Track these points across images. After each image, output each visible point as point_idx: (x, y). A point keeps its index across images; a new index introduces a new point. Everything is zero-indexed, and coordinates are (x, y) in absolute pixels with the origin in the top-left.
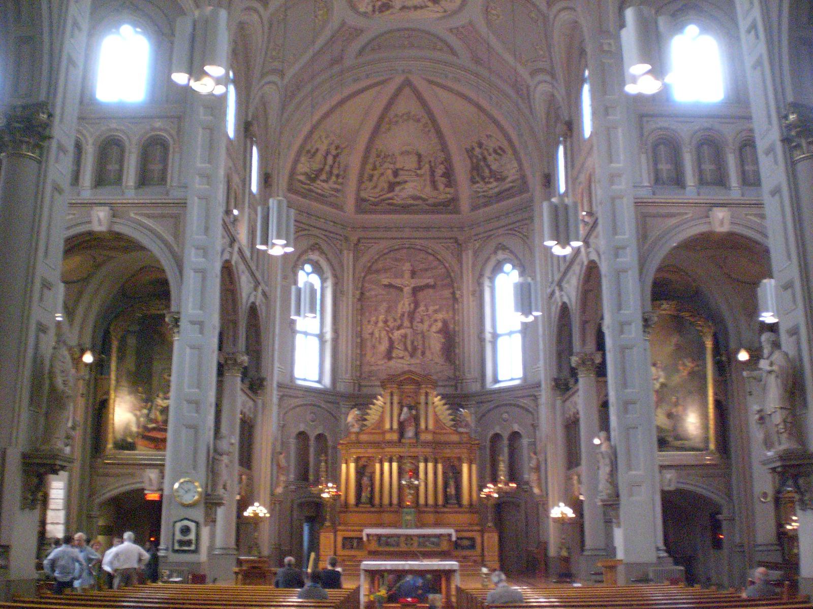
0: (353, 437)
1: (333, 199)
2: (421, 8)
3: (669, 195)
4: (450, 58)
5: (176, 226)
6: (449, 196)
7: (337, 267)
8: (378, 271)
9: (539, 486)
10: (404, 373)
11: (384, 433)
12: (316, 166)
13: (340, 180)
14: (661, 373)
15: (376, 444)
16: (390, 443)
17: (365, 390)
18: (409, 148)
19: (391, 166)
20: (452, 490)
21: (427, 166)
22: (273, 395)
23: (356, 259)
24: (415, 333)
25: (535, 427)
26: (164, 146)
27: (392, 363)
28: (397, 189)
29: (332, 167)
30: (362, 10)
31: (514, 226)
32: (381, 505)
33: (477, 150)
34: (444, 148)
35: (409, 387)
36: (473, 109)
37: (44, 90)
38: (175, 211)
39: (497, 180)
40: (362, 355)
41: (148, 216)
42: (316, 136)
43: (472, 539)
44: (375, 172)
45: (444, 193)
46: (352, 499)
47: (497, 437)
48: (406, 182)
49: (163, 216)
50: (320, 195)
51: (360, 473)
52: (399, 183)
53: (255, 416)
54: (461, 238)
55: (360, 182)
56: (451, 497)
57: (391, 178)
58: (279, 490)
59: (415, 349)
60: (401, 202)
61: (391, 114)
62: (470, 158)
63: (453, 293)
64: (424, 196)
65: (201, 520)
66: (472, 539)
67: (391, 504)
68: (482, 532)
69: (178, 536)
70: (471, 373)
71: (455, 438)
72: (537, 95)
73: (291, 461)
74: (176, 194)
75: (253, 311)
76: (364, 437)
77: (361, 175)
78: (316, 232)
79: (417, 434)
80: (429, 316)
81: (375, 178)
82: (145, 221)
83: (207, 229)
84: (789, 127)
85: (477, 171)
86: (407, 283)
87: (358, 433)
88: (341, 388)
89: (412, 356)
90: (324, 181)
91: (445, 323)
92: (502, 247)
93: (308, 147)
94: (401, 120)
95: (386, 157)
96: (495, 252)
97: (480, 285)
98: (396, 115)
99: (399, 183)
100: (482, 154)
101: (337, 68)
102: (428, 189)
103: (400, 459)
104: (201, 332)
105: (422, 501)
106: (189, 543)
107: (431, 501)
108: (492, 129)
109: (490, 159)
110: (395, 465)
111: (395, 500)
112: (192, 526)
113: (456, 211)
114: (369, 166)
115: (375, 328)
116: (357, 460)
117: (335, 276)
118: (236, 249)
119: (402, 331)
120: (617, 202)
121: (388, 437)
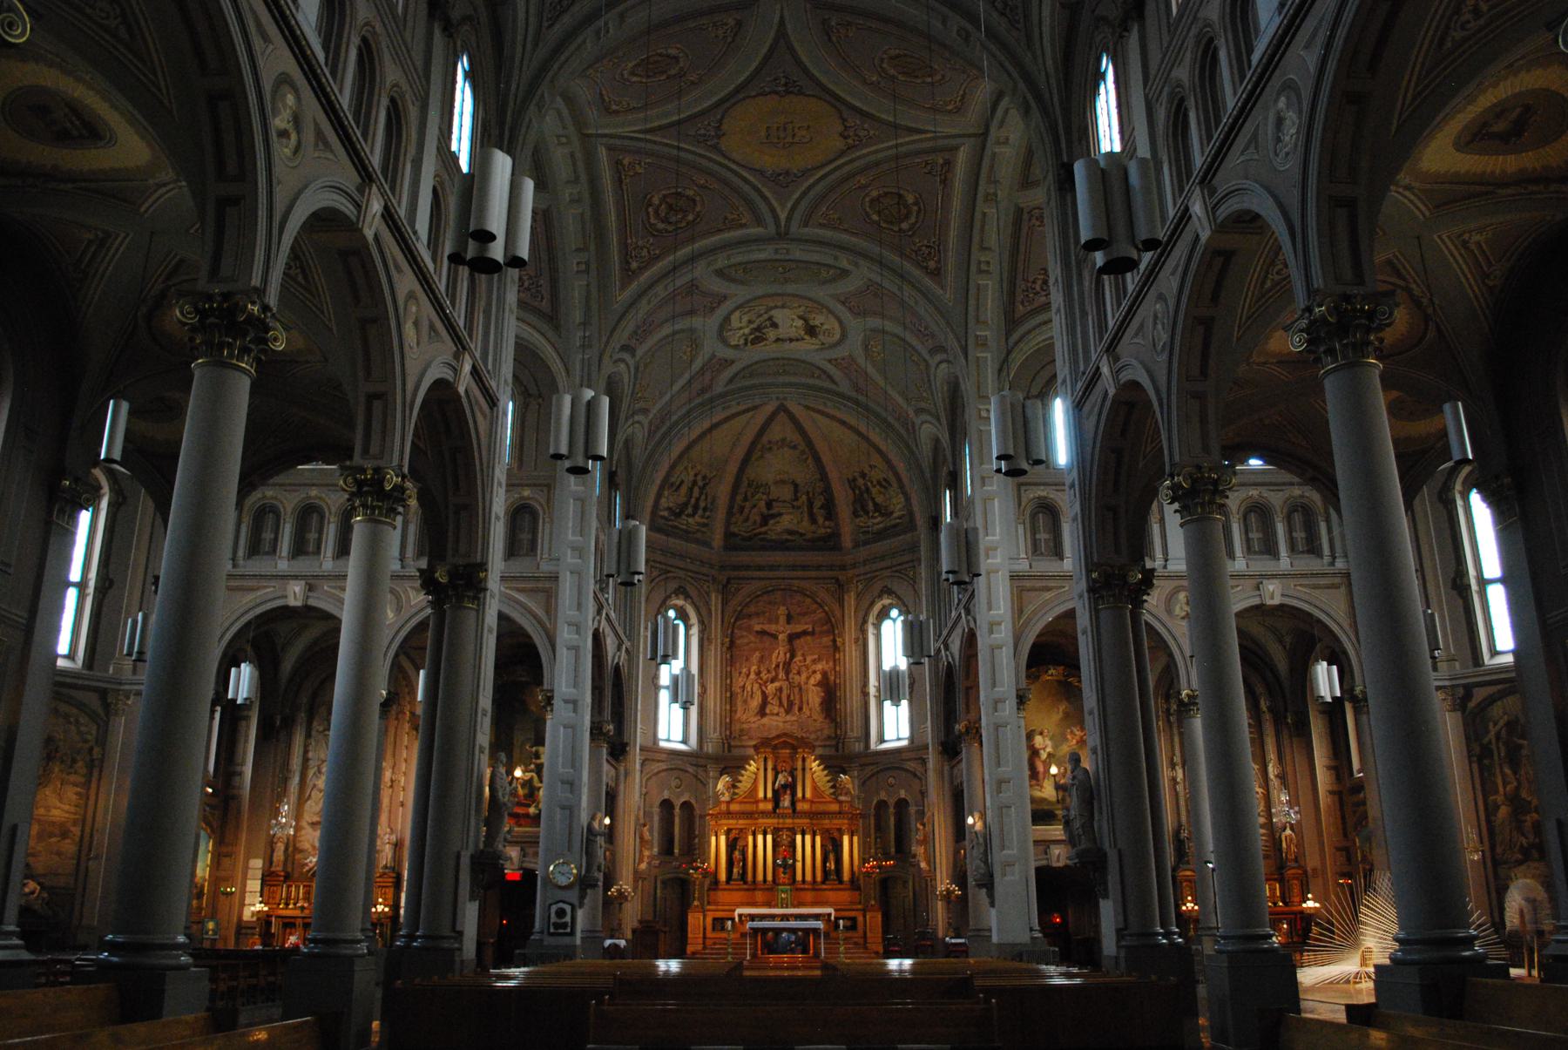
0: (724, 807)
1: (699, 535)
3: (1048, 566)
5: (549, 598)
7: (704, 613)
8: (749, 616)
9: (928, 863)
10: (778, 736)
11: (757, 802)
12: (682, 499)
14: (1049, 743)
15: (749, 815)
16: (764, 814)
17: (736, 752)
20: (832, 865)
22: (636, 757)
23: (725, 603)
24: (791, 686)
25: (923, 794)
26: (534, 515)
27: (765, 720)
29: (698, 500)
32: (754, 881)
33: (860, 481)
34: (824, 477)
35: (783, 749)
38: (547, 585)
39: (882, 515)
40: (732, 711)
41: (519, 590)
42: (680, 468)
43: (854, 920)
44: (747, 504)
46: (723, 876)
47: (882, 805)
48: (780, 515)
51: (731, 846)
52: (773, 516)
53: (617, 784)
55: (730, 513)
56: (831, 875)
57: (764, 510)
58: (643, 866)
59: (791, 704)
61: (765, 439)
63: (834, 641)
65: (576, 903)
66: (854, 920)
67: (765, 880)
68: (864, 911)
69: (553, 919)
70: (855, 732)
71: (835, 807)
73: (653, 834)
74: (546, 567)
75: (617, 669)
76: (734, 807)
77: (731, 507)
78: (681, 574)
79: (793, 803)
80: (807, 667)
82: (521, 597)
83: (579, 606)
85: (861, 505)
86: (782, 630)
87: (728, 803)
88: (709, 748)
89: (788, 711)
91: (824, 674)
92: (887, 591)
95: (758, 487)
96: (880, 596)
97: (863, 632)
101: (707, 396)
103: (776, 832)
104: (575, 711)
105: (799, 877)
106: (564, 925)
107: (809, 877)
108: (876, 459)
109: (874, 491)
110: (769, 838)
111: (770, 878)
112: (568, 908)
113: (837, 547)
114: (739, 498)
115: (747, 680)
116: (728, 832)
117: (701, 622)
118: (467, 368)
119: (777, 684)
121: (762, 806)
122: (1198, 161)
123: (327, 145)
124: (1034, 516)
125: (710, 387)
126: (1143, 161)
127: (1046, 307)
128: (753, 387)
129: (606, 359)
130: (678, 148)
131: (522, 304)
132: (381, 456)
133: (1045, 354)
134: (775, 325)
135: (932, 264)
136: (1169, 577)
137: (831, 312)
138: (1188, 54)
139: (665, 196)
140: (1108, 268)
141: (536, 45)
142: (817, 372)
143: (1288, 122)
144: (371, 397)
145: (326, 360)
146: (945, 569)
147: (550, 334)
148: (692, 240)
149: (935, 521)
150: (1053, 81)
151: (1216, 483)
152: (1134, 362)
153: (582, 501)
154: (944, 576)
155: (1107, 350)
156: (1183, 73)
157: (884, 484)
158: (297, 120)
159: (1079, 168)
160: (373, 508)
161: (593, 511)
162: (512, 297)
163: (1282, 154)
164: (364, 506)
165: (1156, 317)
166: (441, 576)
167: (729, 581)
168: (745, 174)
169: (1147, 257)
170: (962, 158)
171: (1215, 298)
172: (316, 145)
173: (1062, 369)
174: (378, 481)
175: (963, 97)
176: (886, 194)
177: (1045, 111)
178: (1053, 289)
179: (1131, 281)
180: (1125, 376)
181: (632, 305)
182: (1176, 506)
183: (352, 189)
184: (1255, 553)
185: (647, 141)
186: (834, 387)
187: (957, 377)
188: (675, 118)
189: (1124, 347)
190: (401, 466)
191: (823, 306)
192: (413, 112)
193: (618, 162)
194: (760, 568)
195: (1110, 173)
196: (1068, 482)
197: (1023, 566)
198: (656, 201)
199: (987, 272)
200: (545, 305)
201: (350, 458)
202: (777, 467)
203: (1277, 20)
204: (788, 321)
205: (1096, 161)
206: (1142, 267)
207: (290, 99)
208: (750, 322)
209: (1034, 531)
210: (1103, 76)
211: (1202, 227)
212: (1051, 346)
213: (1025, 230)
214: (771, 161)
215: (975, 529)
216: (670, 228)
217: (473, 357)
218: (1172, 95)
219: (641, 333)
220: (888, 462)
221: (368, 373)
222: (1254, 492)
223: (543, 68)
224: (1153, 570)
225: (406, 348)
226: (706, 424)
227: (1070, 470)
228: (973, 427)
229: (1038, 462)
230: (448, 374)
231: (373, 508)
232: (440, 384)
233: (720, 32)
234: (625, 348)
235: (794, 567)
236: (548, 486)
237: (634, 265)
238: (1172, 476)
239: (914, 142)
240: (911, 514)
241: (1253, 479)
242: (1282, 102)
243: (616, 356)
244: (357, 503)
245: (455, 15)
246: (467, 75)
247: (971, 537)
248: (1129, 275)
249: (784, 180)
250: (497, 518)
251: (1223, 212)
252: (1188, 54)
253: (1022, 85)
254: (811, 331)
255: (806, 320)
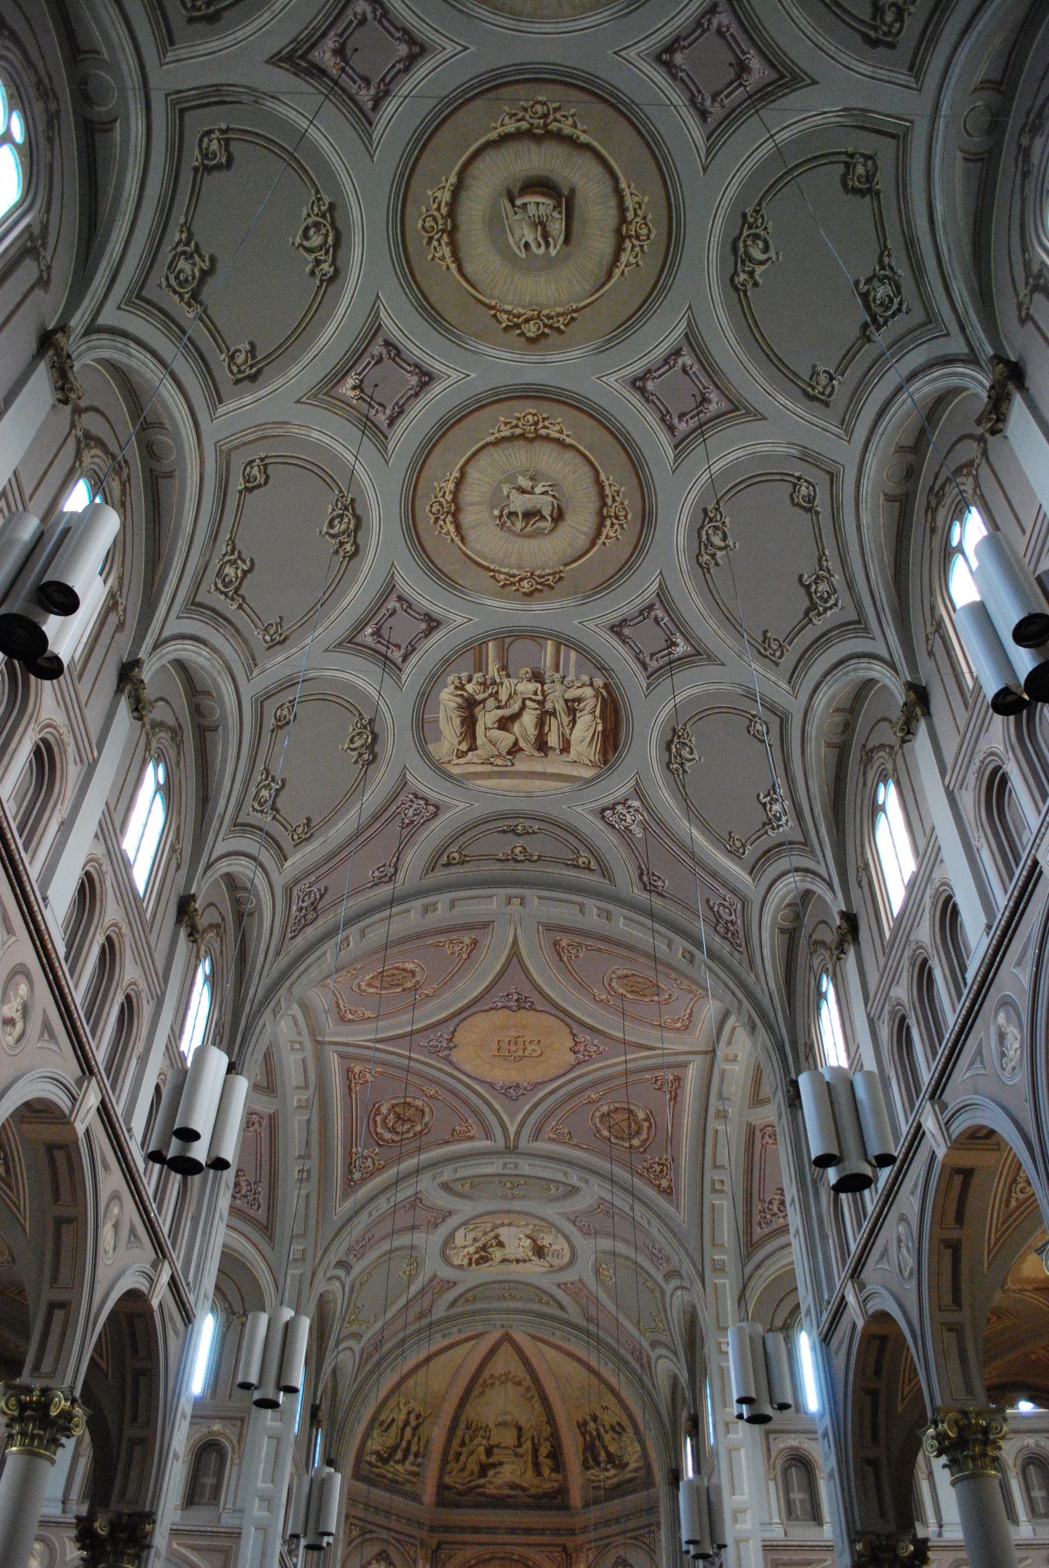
1: (408, 1487)
2: (525, 1261)
3: (804, 1533)
4: (558, 1312)
6: (555, 1484)
12: (390, 1442)
13: (420, 1460)
18: (508, 1418)
19: (484, 1442)
21: (529, 1444)
28: (491, 1473)
29: (409, 1443)
30: (456, 1262)
31: (637, 1533)
33: (592, 1425)
34: (551, 1420)
36: (585, 1373)
37: (148, 1504)
38: (227, 1543)
39: (615, 1466)
41: (193, 1548)
42: (392, 1403)
44: (464, 1449)
45: (549, 1481)
48: (501, 1464)
49: (209, 1549)
50: (391, 1480)
52: (494, 1465)
54: (570, 1545)
55: (445, 1462)
57: (483, 1458)
60: (494, 1491)
61: (486, 1373)
62: (583, 1434)
64: (524, 1484)
72: (659, 1371)
74: (228, 1520)
78: (385, 1534)
81: (463, 1458)
84: (860, 1555)
90: (398, 1462)
93: (382, 1418)
94: (498, 1383)
98: (492, 1376)
99: (494, 1465)
100: (597, 1430)
101: (424, 1322)
102: (530, 1473)
109: (607, 1438)
113: (565, 1507)
114: (456, 1442)
118: (165, 1278)
120: (742, 1546)
122: (926, 1077)
123: (52, 1036)
124: (786, 1471)
125: (430, 1311)
126: (870, 1074)
127: (784, 1229)
128: (474, 1313)
129: (320, 1275)
130: (410, 1058)
131: (234, 1210)
132: (52, 1375)
133: (784, 1286)
134: (501, 1244)
135: (664, 1183)
136: (945, 1548)
137: (560, 1231)
138: (905, 974)
139: (393, 1106)
140: (841, 1187)
141: (278, 953)
142: (545, 1298)
143: (1010, 1037)
144: (53, 1306)
145: (14, 1261)
146: (684, 1537)
147: (263, 1245)
148: (419, 1150)
149: (675, 1475)
150: (777, 1001)
151: (985, 1431)
152: (883, 1291)
153: (277, 1439)
154: (685, 1547)
155: (852, 1277)
156: (902, 992)
157: (618, 1429)
158: (25, 1010)
159: (804, 1081)
160: (33, 1437)
161: (289, 1454)
162: (224, 1202)
163: (1009, 1068)
164: (23, 1434)
165: (899, 1240)
166: (101, 1527)
167: (439, 1544)
168: (477, 1087)
169: (885, 1174)
170: (692, 1075)
171: (960, 1218)
172: (42, 1035)
173: (806, 1298)
174: (44, 1406)
175: (691, 1015)
176: (617, 1109)
177: (770, 1027)
178: (789, 1210)
179: (871, 1199)
180: (873, 1306)
181: (350, 1219)
182: (944, 1459)
183: (70, 1080)
184: (1041, 1516)
185: (377, 1049)
186: (563, 1315)
187: (694, 1306)
188: (409, 1029)
189: (868, 1274)
190: (72, 1388)
191: (552, 1225)
192: (146, 1010)
193: (349, 1070)
194: (476, 1530)
195: (837, 1093)
196: (820, 1431)
197: (777, 1533)
198: (384, 1110)
199: (722, 1191)
200: (261, 1214)
201: (19, 1374)
202: (501, 1407)
203: (986, 941)
204: (516, 1241)
205: (822, 1075)
206: (881, 1184)
207: (23, 989)
208: (475, 1240)
209: (787, 1490)
210: (821, 996)
211: (936, 1143)
212: (792, 1273)
213: (758, 1147)
214: (503, 1074)
215: (719, 1488)
216: (397, 1138)
217: (172, 1265)
218: (893, 1014)
219: (360, 1248)
220: (620, 1401)
221: (55, 1278)
222: (1030, 1441)
223: (285, 975)
224: (926, 1540)
225: (101, 1248)
226: (423, 1354)
227: (822, 1415)
228: (713, 1368)
229: (783, 1407)
230: (142, 1285)
231: (33, 1437)
232: (133, 1295)
233: (457, 949)
234: (340, 1264)
235: (513, 1531)
236: (242, 1420)
237: (357, 1176)
238: (935, 1423)
239: (643, 1058)
240: (648, 1466)
241: (1023, 1426)
242: (1001, 1018)
243: (332, 1272)
244: (17, 1428)
245: (202, 922)
246: (206, 978)
247: (713, 1499)
248: (866, 1192)
249: (512, 1093)
250: (176, 1457)
251: (959, 1127)
252: (905, 974)
253: (746, 1003)
254: (540, 1251)
255: (534, 1241)
